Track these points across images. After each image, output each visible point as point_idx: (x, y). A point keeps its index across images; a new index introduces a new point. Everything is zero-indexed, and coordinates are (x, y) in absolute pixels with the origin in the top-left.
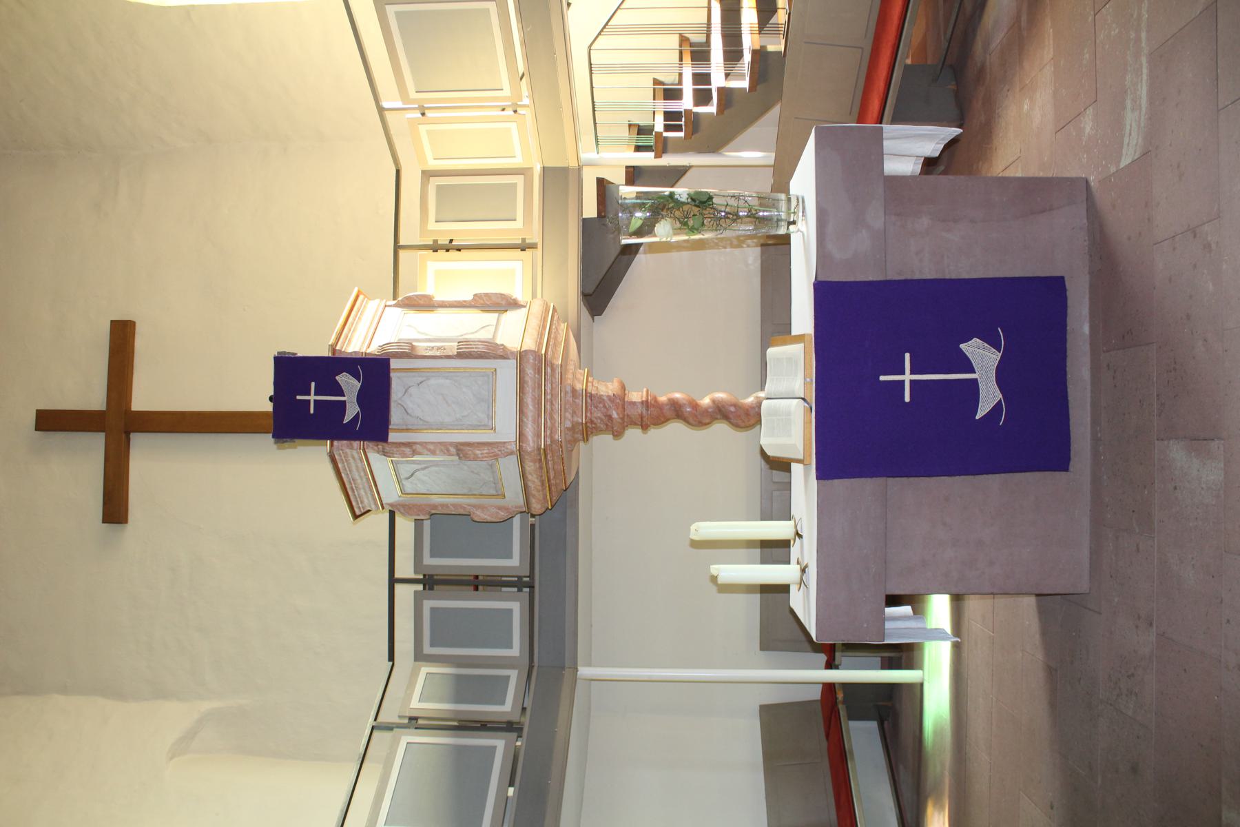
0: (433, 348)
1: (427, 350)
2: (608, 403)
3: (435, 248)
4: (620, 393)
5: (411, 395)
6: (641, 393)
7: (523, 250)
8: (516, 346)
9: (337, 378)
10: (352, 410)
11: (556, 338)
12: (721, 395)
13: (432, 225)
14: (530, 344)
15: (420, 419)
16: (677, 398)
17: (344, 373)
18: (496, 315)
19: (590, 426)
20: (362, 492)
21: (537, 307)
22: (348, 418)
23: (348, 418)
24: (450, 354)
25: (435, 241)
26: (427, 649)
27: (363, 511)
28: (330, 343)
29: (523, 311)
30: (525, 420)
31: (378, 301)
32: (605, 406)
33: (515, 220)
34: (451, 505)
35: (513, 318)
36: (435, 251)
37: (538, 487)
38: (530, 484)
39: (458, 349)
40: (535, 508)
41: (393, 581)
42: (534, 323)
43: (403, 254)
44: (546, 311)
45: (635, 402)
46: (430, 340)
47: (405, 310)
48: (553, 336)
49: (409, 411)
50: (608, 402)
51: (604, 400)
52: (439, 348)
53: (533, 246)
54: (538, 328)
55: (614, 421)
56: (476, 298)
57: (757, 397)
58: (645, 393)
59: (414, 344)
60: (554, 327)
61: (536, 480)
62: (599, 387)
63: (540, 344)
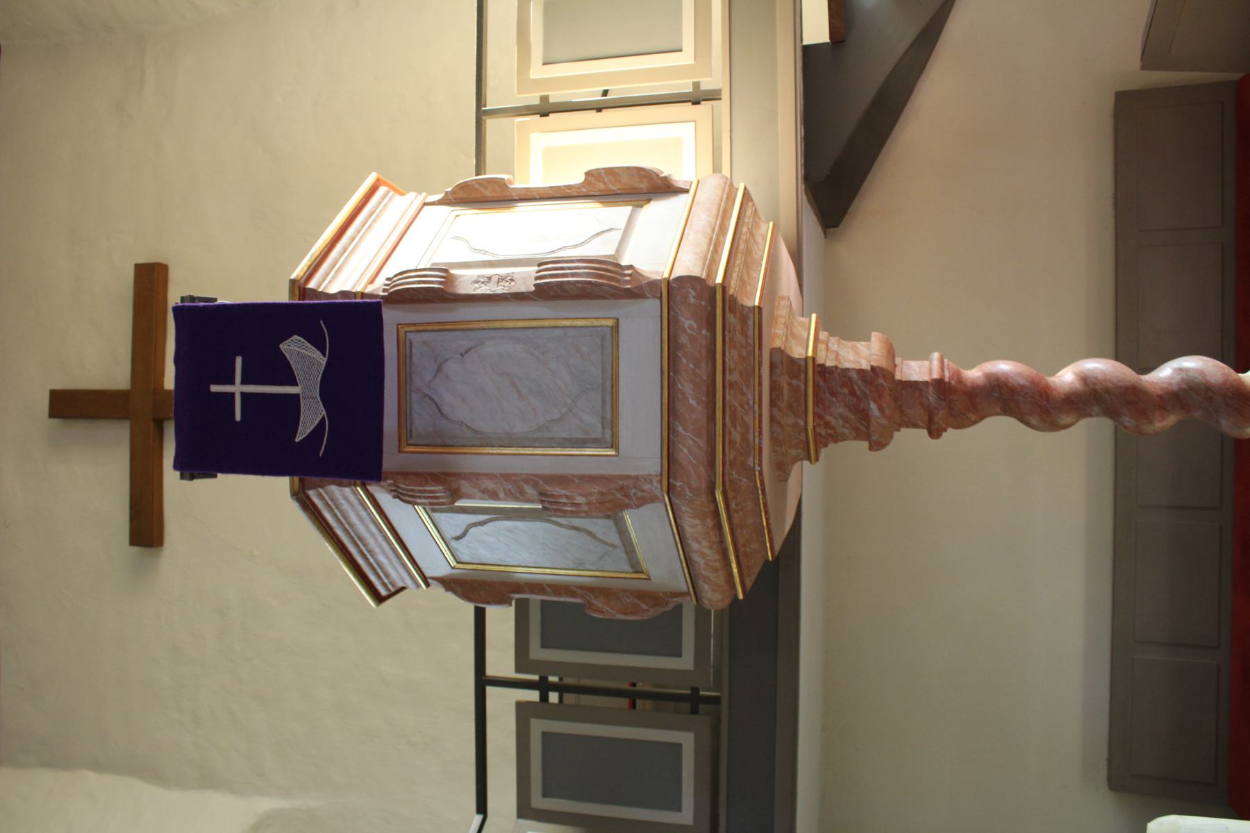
0: (490, 278)
1: (477, 282)
2: (859, 386)
3: (545, 109)
4: (826, 339)
5: (448, 377)
6: (926, 363)
7: (696, 103)
8: (661, 270)
9: (283, 347)
10: (312, 415)
11: (748, 252)
12: (1004, 367)
13: (538, 71)
14: (689, 265)
15: (467, 426)
16: (1006, 374)
17: (296, 337)
18: (626, 210)
19: (823, 433)
20: (382, 558)
21: (710, 192)
22: (304, 431)
23: (304, 431)
24: (523, 289)
25: (544, 99)
26: (538, 801)
27: (393, 590)
28: (293, 276)
29: (682, 201)
30: (680, 429)
31: (412, 195)
32: (853, 393)
33: (681, 51)
34: (547, 585)
35: (659, 211)
36: (545, 114)
37: (713, 564)
38: (696, 558)
39: (537, 278)
40: (710, 600)
41: (482, 682)
42: (703, 220)
43: (491, 124)
44: (728, 198)
45: (916, 383)
46: (490, 264)
47: (458, 210)
48: (742, 247)
49: (446, 410)
50: (859, 382)
51: (850, 379)
52: (501, 279)
53: (713, 96)
54: (709, 231)
55: (873, 420)
56: (589, 178)
57: (1181, 369)
58: (936, 363)
59: (452, 272)
60: (745, 229)
61: (708, 551)
62: (841, 352)
63: (712, 264)
